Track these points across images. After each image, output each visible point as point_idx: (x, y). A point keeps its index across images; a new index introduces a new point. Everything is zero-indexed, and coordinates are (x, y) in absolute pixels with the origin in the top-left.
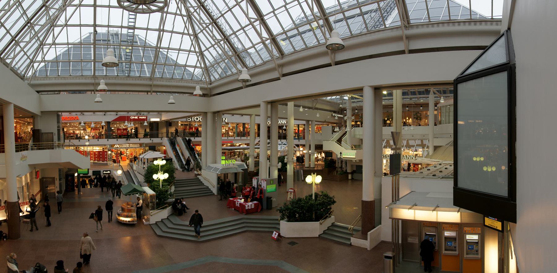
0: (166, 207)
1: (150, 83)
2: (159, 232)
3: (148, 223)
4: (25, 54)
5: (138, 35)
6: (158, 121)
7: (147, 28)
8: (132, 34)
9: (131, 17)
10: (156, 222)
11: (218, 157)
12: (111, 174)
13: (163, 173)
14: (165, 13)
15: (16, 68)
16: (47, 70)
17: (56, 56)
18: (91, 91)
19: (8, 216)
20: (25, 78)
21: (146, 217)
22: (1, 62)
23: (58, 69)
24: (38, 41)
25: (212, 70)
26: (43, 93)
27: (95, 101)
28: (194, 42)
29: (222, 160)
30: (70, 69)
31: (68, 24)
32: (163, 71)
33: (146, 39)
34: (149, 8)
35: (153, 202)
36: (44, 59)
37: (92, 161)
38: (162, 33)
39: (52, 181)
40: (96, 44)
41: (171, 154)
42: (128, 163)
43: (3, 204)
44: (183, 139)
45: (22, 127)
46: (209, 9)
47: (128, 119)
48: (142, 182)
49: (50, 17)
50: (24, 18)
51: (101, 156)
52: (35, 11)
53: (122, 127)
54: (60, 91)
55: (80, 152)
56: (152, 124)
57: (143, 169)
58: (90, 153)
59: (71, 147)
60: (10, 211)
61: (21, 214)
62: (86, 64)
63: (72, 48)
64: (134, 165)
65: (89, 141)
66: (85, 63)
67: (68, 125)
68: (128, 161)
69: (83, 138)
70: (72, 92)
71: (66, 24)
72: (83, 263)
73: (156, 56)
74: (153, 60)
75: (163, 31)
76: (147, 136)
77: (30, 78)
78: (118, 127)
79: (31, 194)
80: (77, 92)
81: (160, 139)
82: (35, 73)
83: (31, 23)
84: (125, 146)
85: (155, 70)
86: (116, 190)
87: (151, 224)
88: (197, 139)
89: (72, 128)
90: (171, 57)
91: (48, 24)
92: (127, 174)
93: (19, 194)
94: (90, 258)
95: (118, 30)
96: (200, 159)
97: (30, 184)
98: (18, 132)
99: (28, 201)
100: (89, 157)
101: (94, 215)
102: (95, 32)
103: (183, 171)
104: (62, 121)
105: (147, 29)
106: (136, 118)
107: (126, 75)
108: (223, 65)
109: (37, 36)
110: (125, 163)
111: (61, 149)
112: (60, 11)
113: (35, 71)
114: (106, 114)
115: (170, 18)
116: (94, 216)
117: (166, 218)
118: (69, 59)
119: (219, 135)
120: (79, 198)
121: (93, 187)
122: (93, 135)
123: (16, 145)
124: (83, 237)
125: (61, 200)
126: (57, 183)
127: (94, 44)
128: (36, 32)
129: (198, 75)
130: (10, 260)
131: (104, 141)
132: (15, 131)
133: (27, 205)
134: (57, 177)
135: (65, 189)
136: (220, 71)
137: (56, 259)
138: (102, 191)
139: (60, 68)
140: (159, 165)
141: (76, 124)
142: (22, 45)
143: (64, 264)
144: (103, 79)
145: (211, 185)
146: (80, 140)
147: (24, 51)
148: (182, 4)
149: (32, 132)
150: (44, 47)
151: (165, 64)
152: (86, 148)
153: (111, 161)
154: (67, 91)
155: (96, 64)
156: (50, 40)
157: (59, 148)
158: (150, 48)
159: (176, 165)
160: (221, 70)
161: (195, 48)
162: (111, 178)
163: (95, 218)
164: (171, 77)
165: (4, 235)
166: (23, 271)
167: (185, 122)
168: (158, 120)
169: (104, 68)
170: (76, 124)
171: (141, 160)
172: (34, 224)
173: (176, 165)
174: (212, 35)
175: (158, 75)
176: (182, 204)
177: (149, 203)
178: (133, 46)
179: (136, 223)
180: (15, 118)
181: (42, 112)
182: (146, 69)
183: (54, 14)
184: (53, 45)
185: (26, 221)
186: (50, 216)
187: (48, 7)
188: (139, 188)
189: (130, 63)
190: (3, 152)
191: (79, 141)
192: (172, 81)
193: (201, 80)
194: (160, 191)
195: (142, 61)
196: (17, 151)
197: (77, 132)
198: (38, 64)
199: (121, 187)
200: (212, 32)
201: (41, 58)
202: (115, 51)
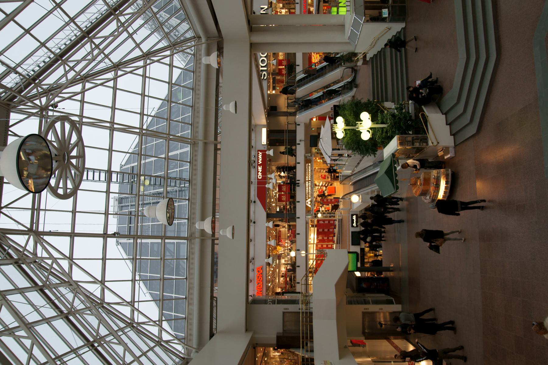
0: (424, 116)
1: (201, 145)
2: (472, 130)
3: (452, 150)
4: (144, 354)
5: (122, 166)
6: (267, 131)
8: (119, 175)
9: (91, 177)
11: (333, 21)
12: (358, 213)
13: (359, 123)
14: (82, 119)
16: (175, 318)
17: (152, 302)
18: (213, 244)
20: (186, 357)
21: (440, 154)
24: (126, 331)
25: (174, 37)
26: (214, 327)
27: (231, 238)
29: (338, 13)
30: (176, 279)
31: (100, 280)
32: (181, 122)
33: (127, 153)
34: (76, 145)
35: (413, 140)
36: (157, 321)
37: (334, 246)
38: (115, 126)
39: (369, 316)
40: (135, 234)
41: (327, 106)
42: (339, 183)
46: (65, 44)
47: (262, 183)
48: (375, 159)
49: (86, 308)
50: (84, 353)
51: (326, 230)
53: (276, 193)
54: (212, 297)
55: (318, 265)
56: (273, 141)
57: (351, 157)
58: (320, 248)
59: (310, 281)
63: (141, 274)
64: (343, 174)
65: (299, 250)
66: (167, 253)
67: (271, 285)
68: (336, 184)
69: (294, 260)
70: (215, 277)
73: (156, 134)
74: (162, 140)
75: (112, 122)
76: (292, 150)
77: (187, 348)
78: (276, 201)
80: (215, 267)
81: (297, 126)
82: (179, 338)
83: (94, 341)
84: (308, 189)
85: (178, 136)
86: (387, 205)
87: (453, 145)
88: (299, 60)
89: (275, 278)
90: (156, 109)
91: (99, 311)
92: (358, 186)
95: (112, 198)
97: (375, 358)
100: (327, 251)
101: (433, 244)
102: (116, 235)
103: (357, 86)
105: (110, 150)
106: (260, 169)
107: (187, 185)
108: (163, 15)
109: (116, 331)
110: (340, 189)
111: (313, 299)
113: (176, 338)
114: (253, 221)
115: (90, 112)
116: (435, 245)
117: (444, 116)
119: (292, 20)
120: (400, 269)
122: (289, 242)
128: (111, 334)
129: (185, 60)
131: (300, 225)
134: (361, 308)
135: (383, 295)
136: (174, 21)
139: (174, 295)
140: (345, 130)
141: (270, 270)
144: (194, 223)
145: (384, 34)
146: (297, 265)
147: (141, 356)
148: (63, 92)
149: (281, 349)
150: (136, 321)
151: (169, 119)
152: (311, 256)
154: (213, 285)
155: (168, 235)
156: (126, 311)
157: (310, 303)
158: (141, 146)
159: (345, 98)
160: (173, 18)
161: (138, 68)
162: (365, 213)
163: (438, 243)
164: (191, 109)
167: (269, 82)
168: (264, 131)
169: (175, 222)
170: (270, 270)
171: (335, 160)
173: (345, 98)
174: (111, 38)
175: (187, 132)
176: (421, 86)
177: (414, 148)
179: (450, 170)
181: (247, 330)
183: (82, 302)
184: (133, 306)
187: (70, 311)
188: (386, 166)
189: (168, 178)
191: (299, 266)
192: (198, 108)
193: (194, 55)
194: (392, 126)
195: (165, 158)
197: (283, 269)
199: (382, 196)
200: (106, 38)
201: (155, 327)
202: (147, 204)
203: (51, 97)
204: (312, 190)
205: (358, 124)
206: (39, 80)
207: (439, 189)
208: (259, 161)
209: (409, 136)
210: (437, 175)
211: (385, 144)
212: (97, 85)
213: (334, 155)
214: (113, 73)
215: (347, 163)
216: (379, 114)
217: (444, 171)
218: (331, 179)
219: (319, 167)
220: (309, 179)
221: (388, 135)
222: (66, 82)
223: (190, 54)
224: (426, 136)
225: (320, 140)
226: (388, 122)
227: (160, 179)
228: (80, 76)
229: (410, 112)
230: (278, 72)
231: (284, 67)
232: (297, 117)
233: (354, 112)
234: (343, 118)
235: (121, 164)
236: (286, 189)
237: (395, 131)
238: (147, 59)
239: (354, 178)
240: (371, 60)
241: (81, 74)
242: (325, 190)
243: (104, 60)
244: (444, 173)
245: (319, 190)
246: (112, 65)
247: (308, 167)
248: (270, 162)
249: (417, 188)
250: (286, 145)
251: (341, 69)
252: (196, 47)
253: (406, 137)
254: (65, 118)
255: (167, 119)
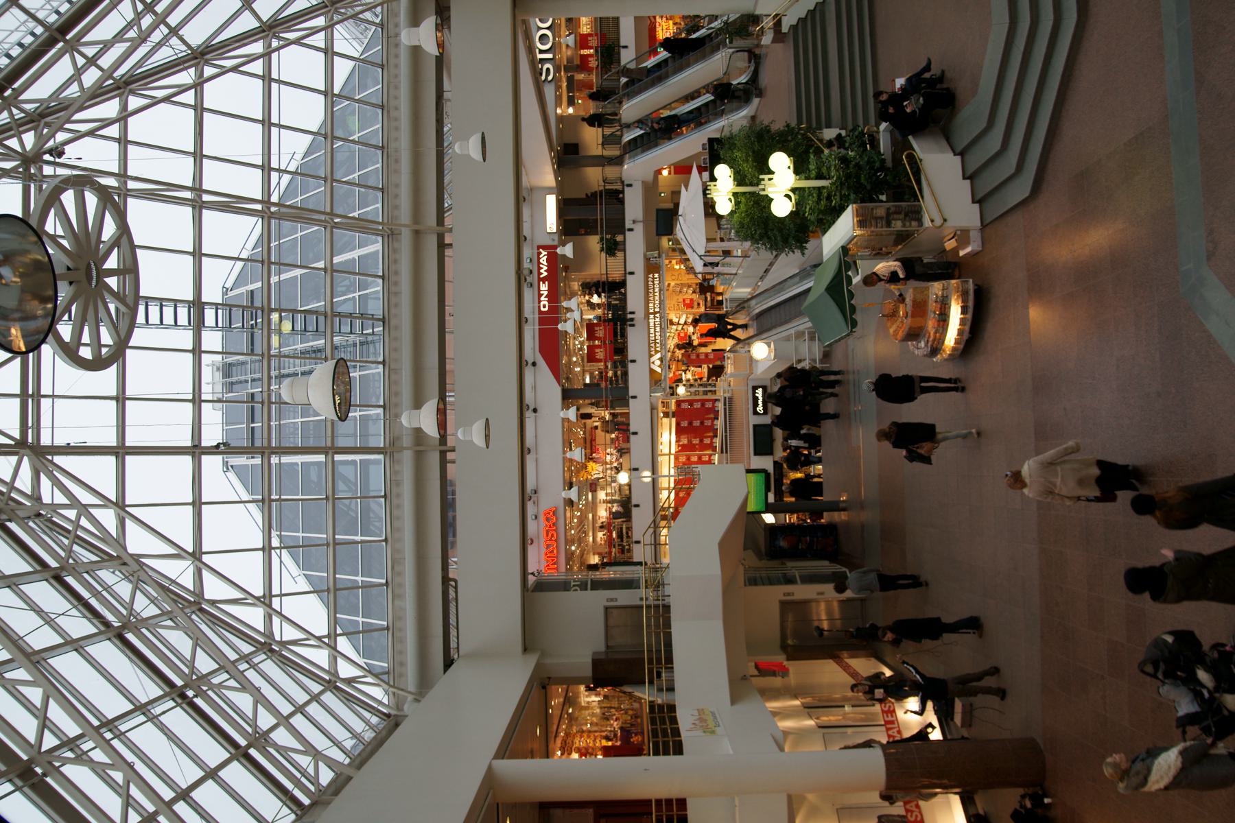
3: (975, 236)
4: (300, 709)
5: (226, 291)
6: (558, 201)
7: (193, 254)
8: (220, 312)
9: (154, 317)
10: (973, 202)
12: (768, 383)
13: (766, 177)
15: (354, 747)
17: (312, 595)
18: (444, 463)
19: (947, 788)
20: (393, 712)
21: (950, 245)
22: (328, 803)
23: (362, 587)
24: (256, 660)
26: (453, 645)
28: (228, 63)
30: (362, 542)
31: (191, 550)
32: (359, 185)
34: (116, 243)
35: (888, 214)
36: (324, 637)
37: (716, 458)
38: (206, 198)
40: (265, 444)
41: (691, 144)
43: (898, 809)
44: (630, 96)
45: (584, 728)
47: (550, 319)
50: (164, 713)
51: (697, 423)
52: (136, 668)
53: (582, 343)
54: (446, 580)
55: (680, 502)
56: (571, 225)
58: (684, 464)
59: (663, 538)
60: (926, 781)
61: (936, 735)
62: (344, 483)
65: (636, 469)
66: (341, 486)
67: (577, 548)
69: (627, 492)
70: (451, 535)
71: (193, 555)
72: (1135, 489)
73: (301, 215)
74: (316, 228)
75: (198, 189)
77: (394, 694)
78: (583, 360)
79: (850, 694)
80: (450, 514)
83: (186, 686)
84: (656, 333)
87: (979, 225)
88: (627, 35)
90: (299, 156)
91: (192, 620)
93: (850, 743)
94: (1116, 465)
95: (208, 365)
96: (710, 22)
97: (808, 700)
98: (604, 743)
99: (877, 708)
103: (760, 94)
104: (560, 573)
106: (544, 288)
107: (379, 329)
109: (234, 662)
112: (144, 577)
113: (369, 672)
114: (532, 408)
115: (141, 164)
117: (958, 158)
118: (323, 545)
120: (862, 506)
121: (819, 451)
122: (614, 452)
123: (656, 753)
124: (1026, 491)
125: (873, 577)
126: (802, 592)
127: (266, 451)
130: (1135, 781)
132: (600, 757)
133: (894, 711)
134: (777, 593)
135: (826, 563)
137: (1118, 596)
138: (835, 416)
139: (359, 579)
140: (735, 194)
142: (265, 720)
143: (1140, 564)
144: (398, 416)
146: (634, 502)
147: (292, 714)
149: (603, 687)
150: (278, 638)
151: (330, 179)
153: (715, 386)
156: (254, 617)
157: (663, 585)
158: (269, 242)
159: (735, 120)
161: (252, 59)
164: (379, 152)
165: (1028, 804)
166: (1178, 727)
167: (558, 88)
168: (551, 202)
169: (355, 414)
170: (573, 517)
172: (975, 684)
175: (374, 208)
176: (907, 92)
178: (266, 307)
179: (971, 280)
180: (548, 757)
181: (525, 650)
182: (355, 254)
184: (270, 606)
185: (964, 713)
186: (939, 619)
187: (125, 620)
190: (682, 803)
191: (637, 506)
193: (381, 25)
194: (842, 184)
195: (325, 270)
196: (679, 750)
197: (603, 513)
198: (340, 661)
201: (320, 651)
202: (288, 376)
203: (45, 131)
204: (663, 335)
205: (763, 180)
206: (13, 89)
207: (948, 325)
208: (542, 271)
209: (881, 206)
210: (943, 294)
211: (827, 226)
212: (156, 102)
213: (712, 254)
214: (192, 71)
215: (740, 272)
216: (812, 157)
217: (956, 283)
218: (706, 308)
219: (679, 282)
220: (655, 308)
221: (833, 204)
222: (79, 94)
223: (373, 23)
224: (915, 206)
225: (678, 219)
226: (832, 174)
227: (317, 318)
228: (113, 79)
229: (882, 151)
230: (579, 63)
231: (592, 51)
232: (626, 167)
233: (754, 152)
234: (731, 167)
235: (223, 287)
236: (605, 334)
237: (849, 195)
238: (272, 38)
239: (756, 304)
240: (791, 31)
241: (115, 75)
242: (693, 334)
243: (168, 41)
244: (958, 288)
245: (679, 334)
246: (189, 52)
247: (653, 282)
248: (566, 272)
249: (898, 323)
250: (602, 233)
251: (724, 54)
252: (385, 5)
253: (872, 209)
254: (84, 180)
255: (325, 179)
